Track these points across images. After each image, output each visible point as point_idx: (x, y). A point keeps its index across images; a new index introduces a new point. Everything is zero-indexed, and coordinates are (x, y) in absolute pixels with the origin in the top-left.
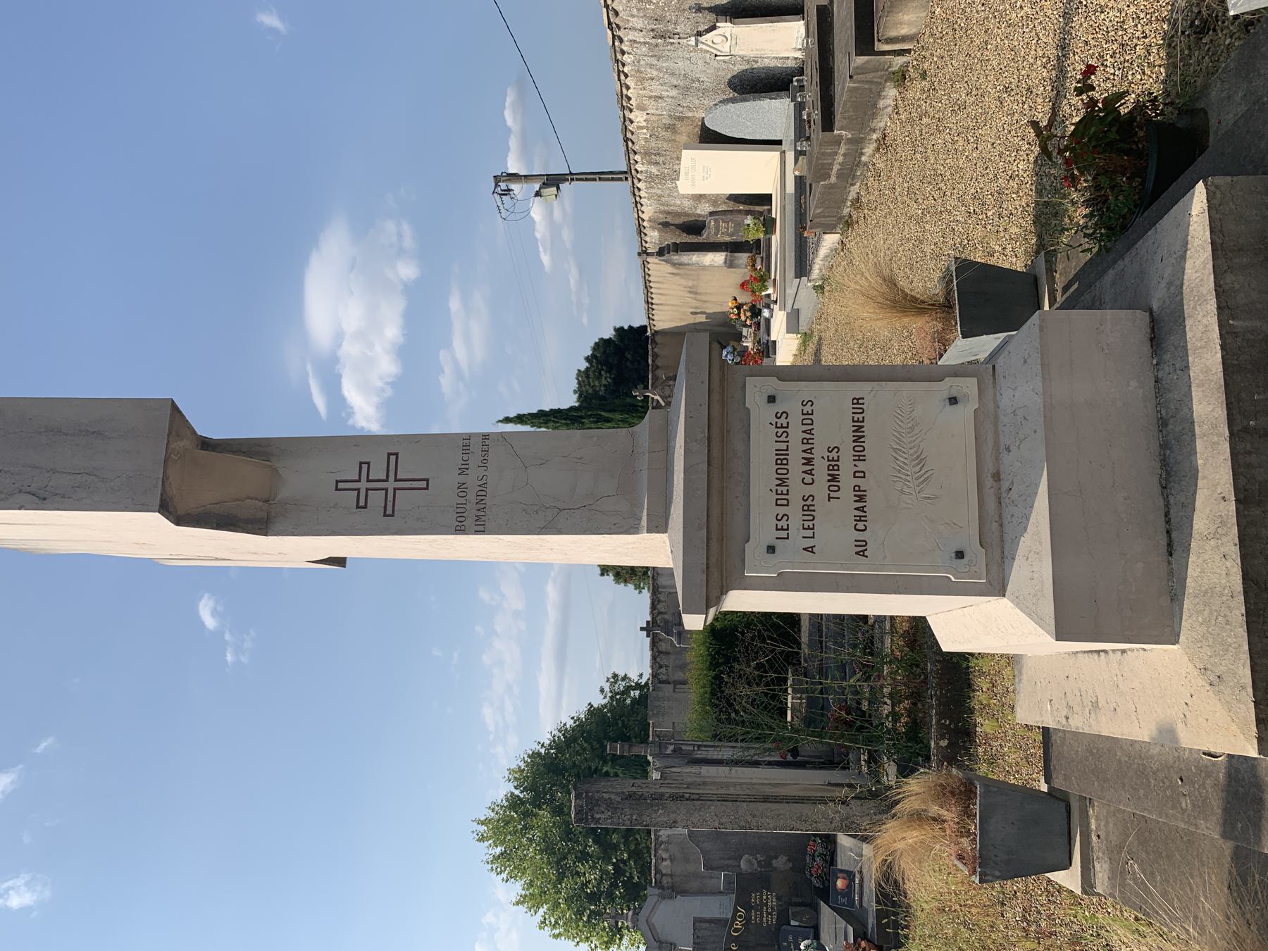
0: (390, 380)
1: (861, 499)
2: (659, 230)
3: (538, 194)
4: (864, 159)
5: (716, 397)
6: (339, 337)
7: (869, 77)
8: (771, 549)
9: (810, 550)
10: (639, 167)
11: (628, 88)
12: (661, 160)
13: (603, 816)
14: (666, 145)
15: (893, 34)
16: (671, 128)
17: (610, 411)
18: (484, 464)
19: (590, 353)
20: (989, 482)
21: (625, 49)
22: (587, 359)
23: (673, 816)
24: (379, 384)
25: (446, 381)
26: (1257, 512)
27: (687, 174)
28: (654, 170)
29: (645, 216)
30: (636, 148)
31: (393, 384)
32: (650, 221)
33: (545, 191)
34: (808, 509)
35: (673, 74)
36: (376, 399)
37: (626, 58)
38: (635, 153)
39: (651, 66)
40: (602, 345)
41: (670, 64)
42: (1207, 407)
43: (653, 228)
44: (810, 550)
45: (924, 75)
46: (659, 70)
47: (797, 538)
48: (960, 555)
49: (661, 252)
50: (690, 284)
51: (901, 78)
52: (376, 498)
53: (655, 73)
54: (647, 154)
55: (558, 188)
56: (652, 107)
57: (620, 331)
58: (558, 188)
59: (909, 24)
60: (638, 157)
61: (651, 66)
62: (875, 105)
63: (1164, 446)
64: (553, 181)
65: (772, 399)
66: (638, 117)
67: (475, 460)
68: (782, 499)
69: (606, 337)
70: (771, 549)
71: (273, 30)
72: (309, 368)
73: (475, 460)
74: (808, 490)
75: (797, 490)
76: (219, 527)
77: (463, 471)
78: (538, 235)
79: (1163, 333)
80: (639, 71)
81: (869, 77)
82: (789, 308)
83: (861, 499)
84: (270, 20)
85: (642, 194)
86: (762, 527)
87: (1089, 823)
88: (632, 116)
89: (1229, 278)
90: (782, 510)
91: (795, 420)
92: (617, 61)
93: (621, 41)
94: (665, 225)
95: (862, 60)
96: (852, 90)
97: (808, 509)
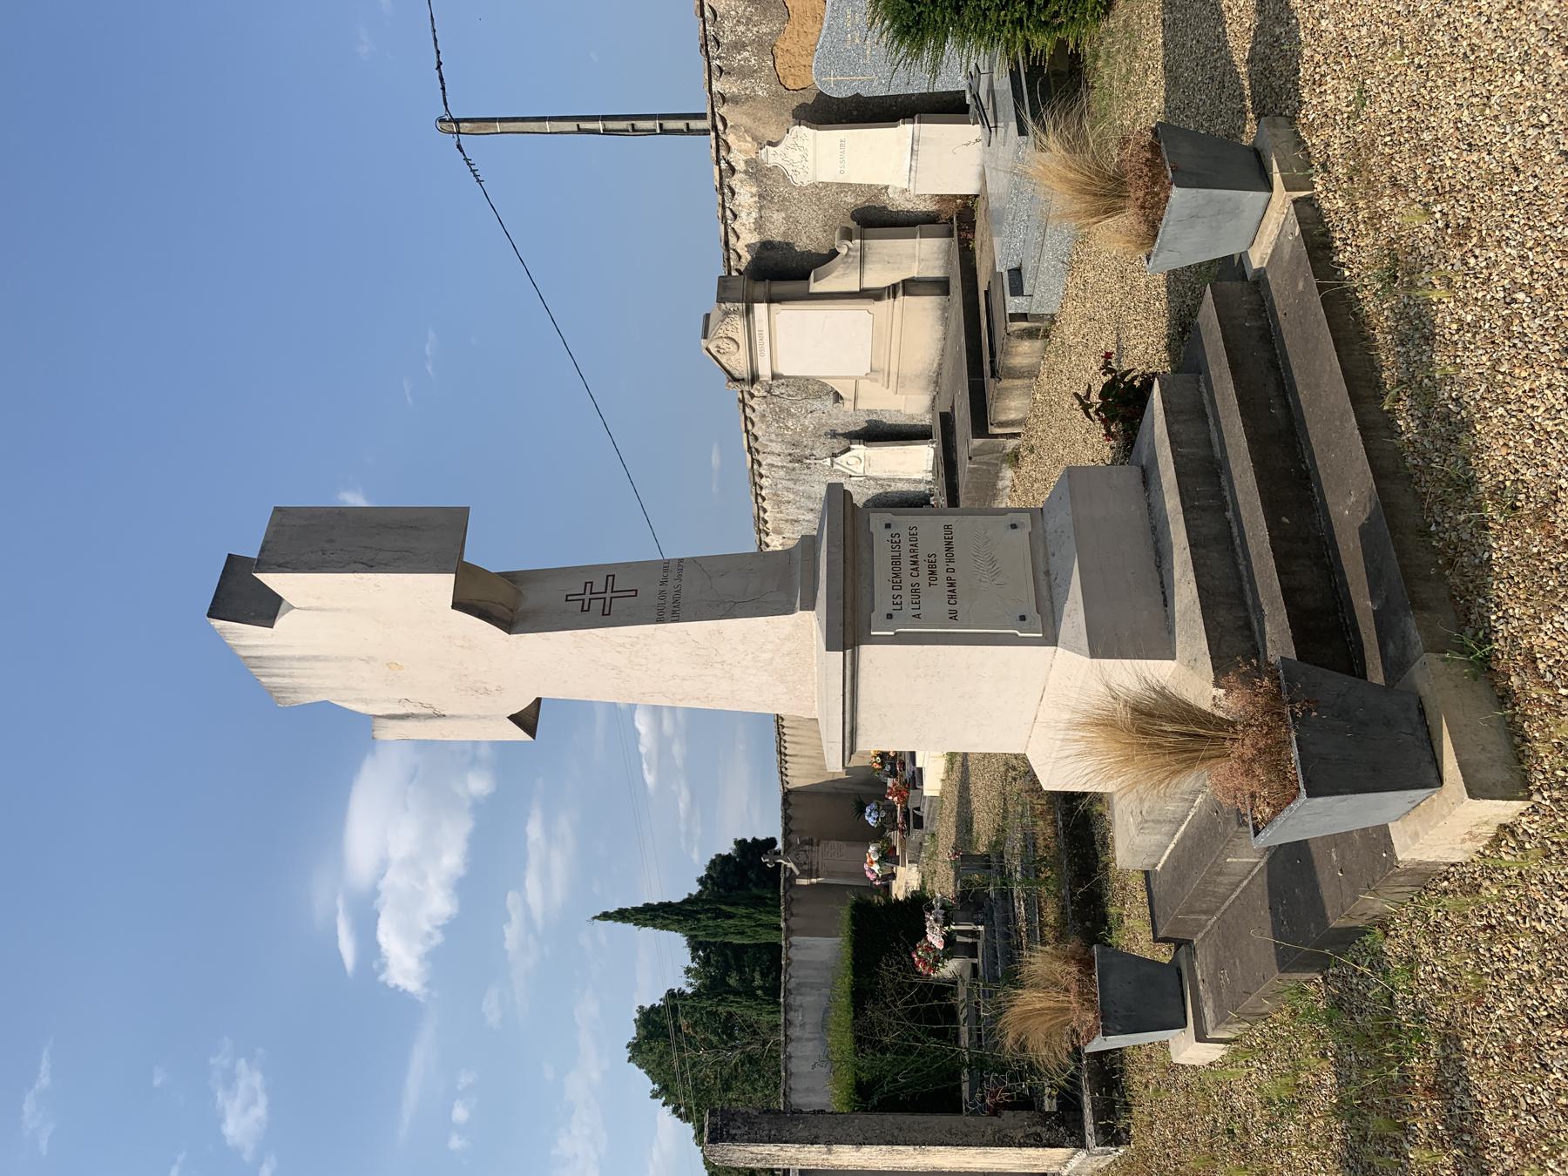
0: (440, 923)
1: (952, 585)
5: (848, 522)
6: (383, 865)
7: (986, 458)
8: (890, 616)
9: (917, 616)
11: (765, 511)
13: (738, 1132)
15: (1003, 418)
17: (732, 905)
18: (679, 578)
19: (704, 873)
20: (1042, 577)
22: (701, 881)
23: (814, 1131)
24: (427, 927)
25: (512, 934)
26: (1203, 551)
31: (445, 929)
34: (915, 591)
36: (419, 948)
37: (764, 482)
39: (788, 490)
40: (720, 863)
41: (806, 487)
42: (1172, 503)
44: (917, 616)
45: (1032, 451)
46: (795, 493)
47: (908, 608)
48: (1023, 618)
51: (1014, 459)
52: (597, 605)
56: (787, 528)
57: (741, 844)
59: (1016, 410)
61: (788, 490)
62: (994, 485)
63: (1156, 543)
65: (888, 526)
67: (672, 576)
68: (897, 585)
69: (725, 852)
70: (890, 616)
72: (340, 903)
73: (672, 576)
74: (915, 580)
75: (907, 581)
76: (479, 616)
77: (662, 583)
78: (643, 750)
79: (1148, 477)
80: (776, 494)
81: (986, 458)
83: (952, 585)
86: (883, 598)
88: (768, 540)
89: (1176, 427)
90: (896, 593)
91: (905, 537)
93: (760, 465)
95: (978, 442)
96: (972, 471)
97: (915, 591)
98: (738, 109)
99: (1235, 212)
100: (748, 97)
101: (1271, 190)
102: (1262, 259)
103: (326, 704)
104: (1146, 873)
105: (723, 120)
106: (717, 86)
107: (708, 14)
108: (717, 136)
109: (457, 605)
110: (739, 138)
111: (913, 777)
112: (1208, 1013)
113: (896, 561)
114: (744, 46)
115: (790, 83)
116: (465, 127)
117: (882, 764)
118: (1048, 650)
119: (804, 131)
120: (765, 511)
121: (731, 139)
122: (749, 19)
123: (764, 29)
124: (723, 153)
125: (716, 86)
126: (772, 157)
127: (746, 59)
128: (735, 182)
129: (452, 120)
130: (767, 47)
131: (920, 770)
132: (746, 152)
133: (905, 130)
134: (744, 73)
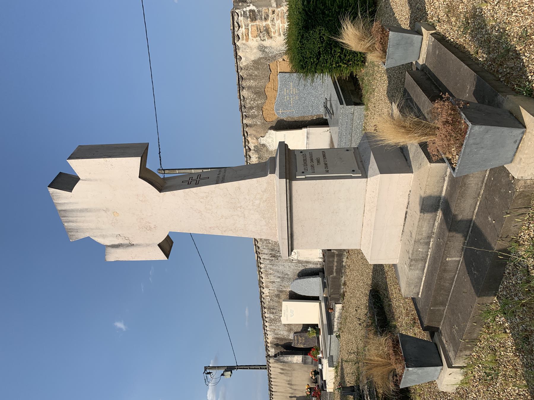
2: (275, 348)
3: (223, 375)
4: (344, 264)
8: (303, 172)
10: (266, 315)
12: (274, 311)
14: (276, 304)
16: (278, 296)
21: (261, 262)
27: (284, 313)
28: (272, 316)
29: (269, 341)
30: (265, 306)
32: (271, 343)
33: (226, 373)
34: (312, 166)
35: (278, 272)
37: (262, 266)
38: (265, 308)
39: (270, 269)
43: (272, 347)
49: (275, 356)
50: (288, 379)
53: (272, 271)
54: (269, 308)
55: (231, 372)
58: (231, 372)
60: (266, 310)
61: (270, 269)
64: (230, 369)
66: (266, 291)
70: (303, 172)
71: (120, 329)
82: (328, 356)
84: (120, 325)
85: (268, 329)
87: (442, 341)
88: (263, 291)
92: (259, 266)
94: (277, 345)
97: (312, 166)
98: (251, 129)
99: (411, 44)
100: (255, 125)
101: (422, 35)
102: (423, 60)
103: (88, 240)
104: (413, 299)
105: (247, 132)
106: (245, 121)
107: (242, 98)
108: (245, 138)
109: (140, 177)
110: (252, 139)
111: (322, 386)
112: (451, 354)
113: (305, 160)
114: (253, 108)
115: (268, 120)
116: (167, 172)
117: (310, 392)
118: (364, 180)
119: (272, 132)
120: (262, 278)
121: (249, 139)
122: (255, 99)
123: (259, 102)
124: (247, 144)
125: (245, 121)
126: (263, 141)
127: (254, 112)
128: (251, 153)
129: (163, 170)
130: (260, 108)
131: (325, 381)
132: (254, 143)
133: (305, 130)
134: (253, 117)
